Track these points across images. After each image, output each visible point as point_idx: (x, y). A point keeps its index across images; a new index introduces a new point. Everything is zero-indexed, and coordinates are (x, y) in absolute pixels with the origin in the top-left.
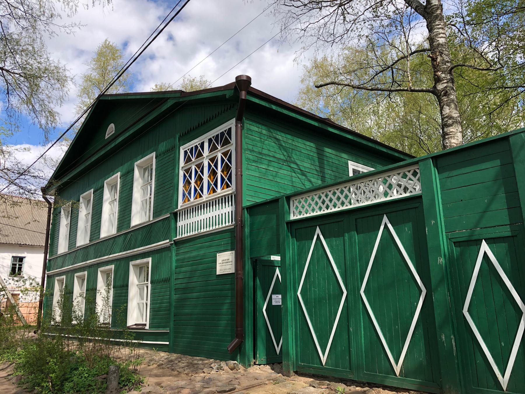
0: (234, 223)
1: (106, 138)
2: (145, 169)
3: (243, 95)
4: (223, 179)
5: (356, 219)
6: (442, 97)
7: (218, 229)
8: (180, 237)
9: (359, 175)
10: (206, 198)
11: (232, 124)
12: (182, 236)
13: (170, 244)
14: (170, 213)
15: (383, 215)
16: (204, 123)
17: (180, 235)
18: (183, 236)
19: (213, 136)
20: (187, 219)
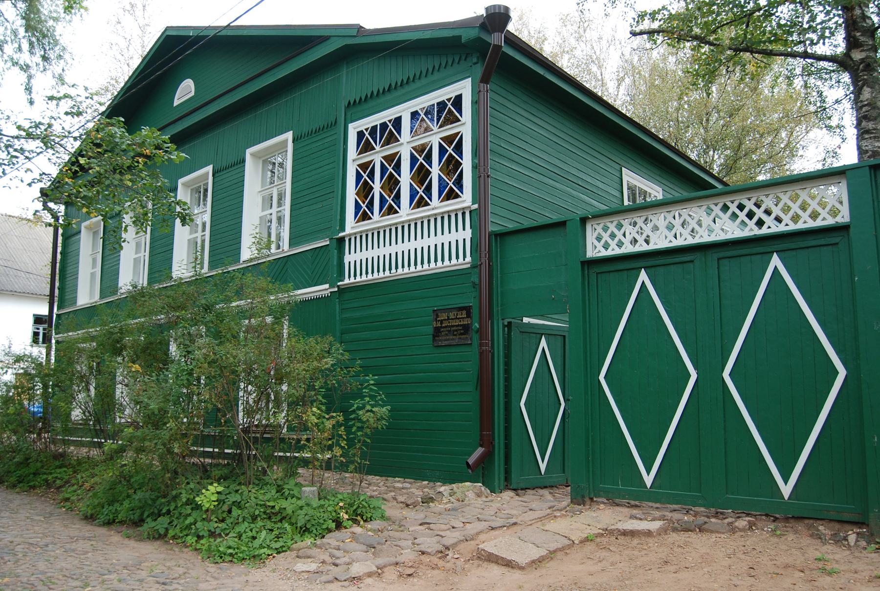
0: (468, 259)
1: (175, 104)
2: (268, 163)
3: (496, 39)
4: (383, 200)
5: (718, 259)
6: (860, 72)
7: (455, 265)
8: (352, 280)
9: (623, 208)
10: (408, 215)
11: (465, 88)
12: (355, 279)
13: (331, 292)
14: (331, 239)
15: (641, 268)
16: (389, 90)
17: (394, 270)
18: (358, 279)
19: (366, 127)
20: (350, 253)
